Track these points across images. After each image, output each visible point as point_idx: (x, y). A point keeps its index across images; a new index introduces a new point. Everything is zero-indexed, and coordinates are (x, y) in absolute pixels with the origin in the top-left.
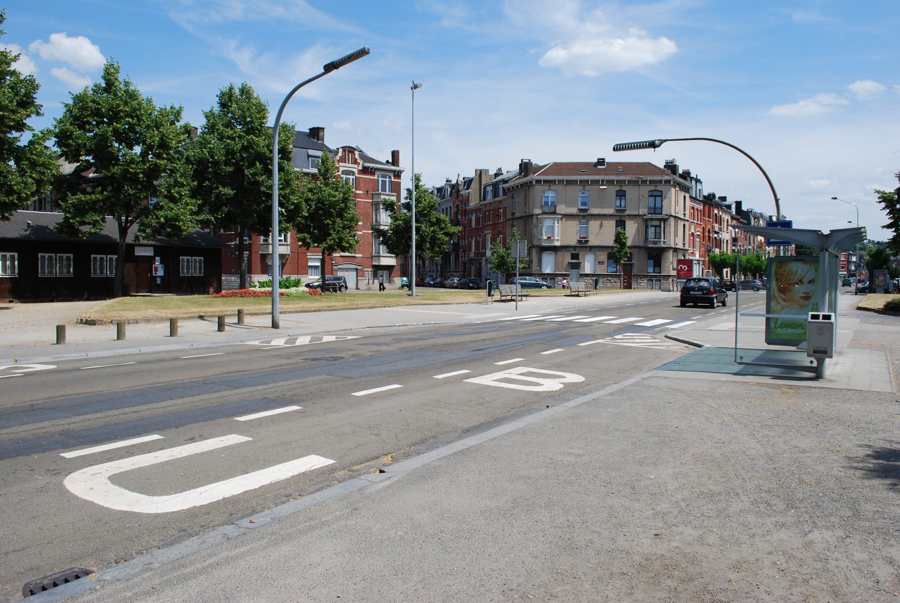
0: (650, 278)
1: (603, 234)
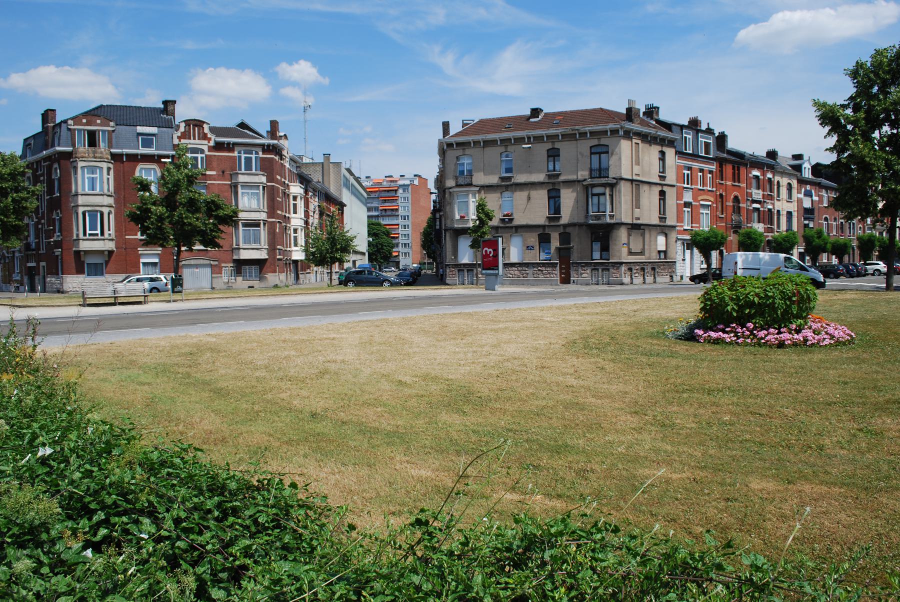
0: (595, 267)
1: (532, 209)
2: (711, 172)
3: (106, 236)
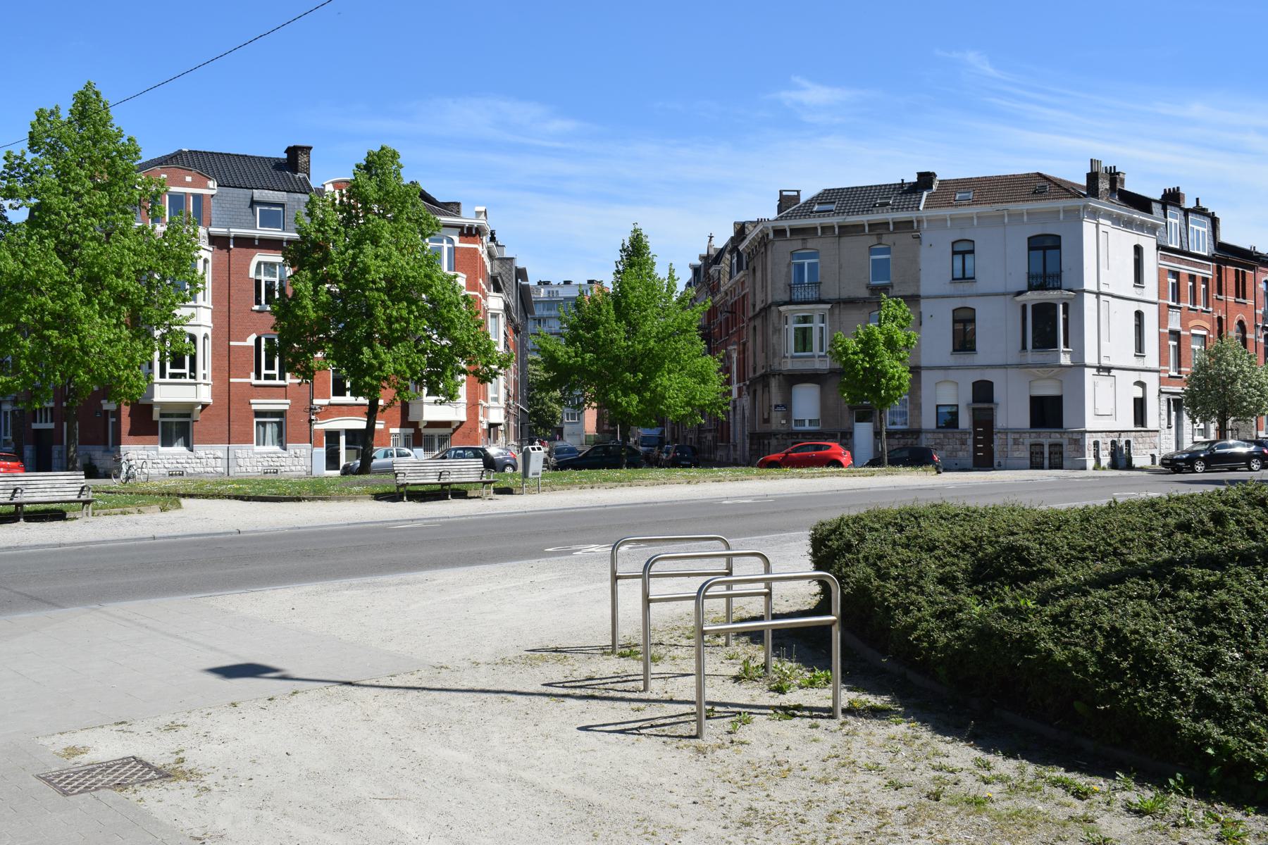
2: (1205, 280)
3: (200, 379)
